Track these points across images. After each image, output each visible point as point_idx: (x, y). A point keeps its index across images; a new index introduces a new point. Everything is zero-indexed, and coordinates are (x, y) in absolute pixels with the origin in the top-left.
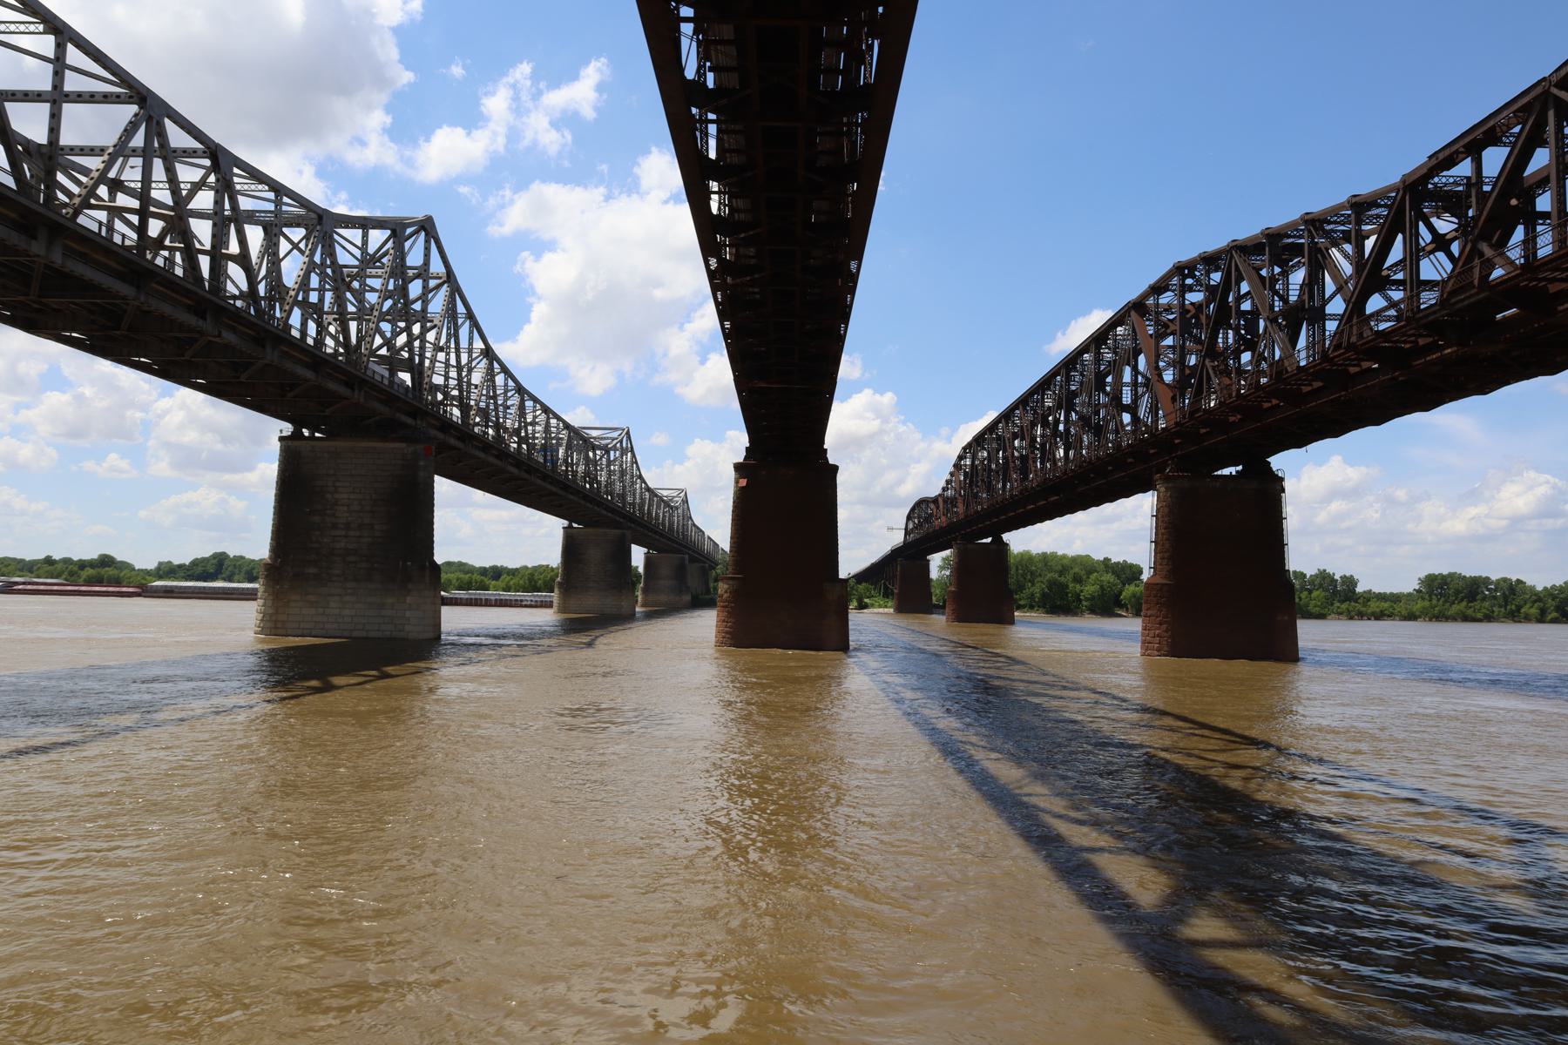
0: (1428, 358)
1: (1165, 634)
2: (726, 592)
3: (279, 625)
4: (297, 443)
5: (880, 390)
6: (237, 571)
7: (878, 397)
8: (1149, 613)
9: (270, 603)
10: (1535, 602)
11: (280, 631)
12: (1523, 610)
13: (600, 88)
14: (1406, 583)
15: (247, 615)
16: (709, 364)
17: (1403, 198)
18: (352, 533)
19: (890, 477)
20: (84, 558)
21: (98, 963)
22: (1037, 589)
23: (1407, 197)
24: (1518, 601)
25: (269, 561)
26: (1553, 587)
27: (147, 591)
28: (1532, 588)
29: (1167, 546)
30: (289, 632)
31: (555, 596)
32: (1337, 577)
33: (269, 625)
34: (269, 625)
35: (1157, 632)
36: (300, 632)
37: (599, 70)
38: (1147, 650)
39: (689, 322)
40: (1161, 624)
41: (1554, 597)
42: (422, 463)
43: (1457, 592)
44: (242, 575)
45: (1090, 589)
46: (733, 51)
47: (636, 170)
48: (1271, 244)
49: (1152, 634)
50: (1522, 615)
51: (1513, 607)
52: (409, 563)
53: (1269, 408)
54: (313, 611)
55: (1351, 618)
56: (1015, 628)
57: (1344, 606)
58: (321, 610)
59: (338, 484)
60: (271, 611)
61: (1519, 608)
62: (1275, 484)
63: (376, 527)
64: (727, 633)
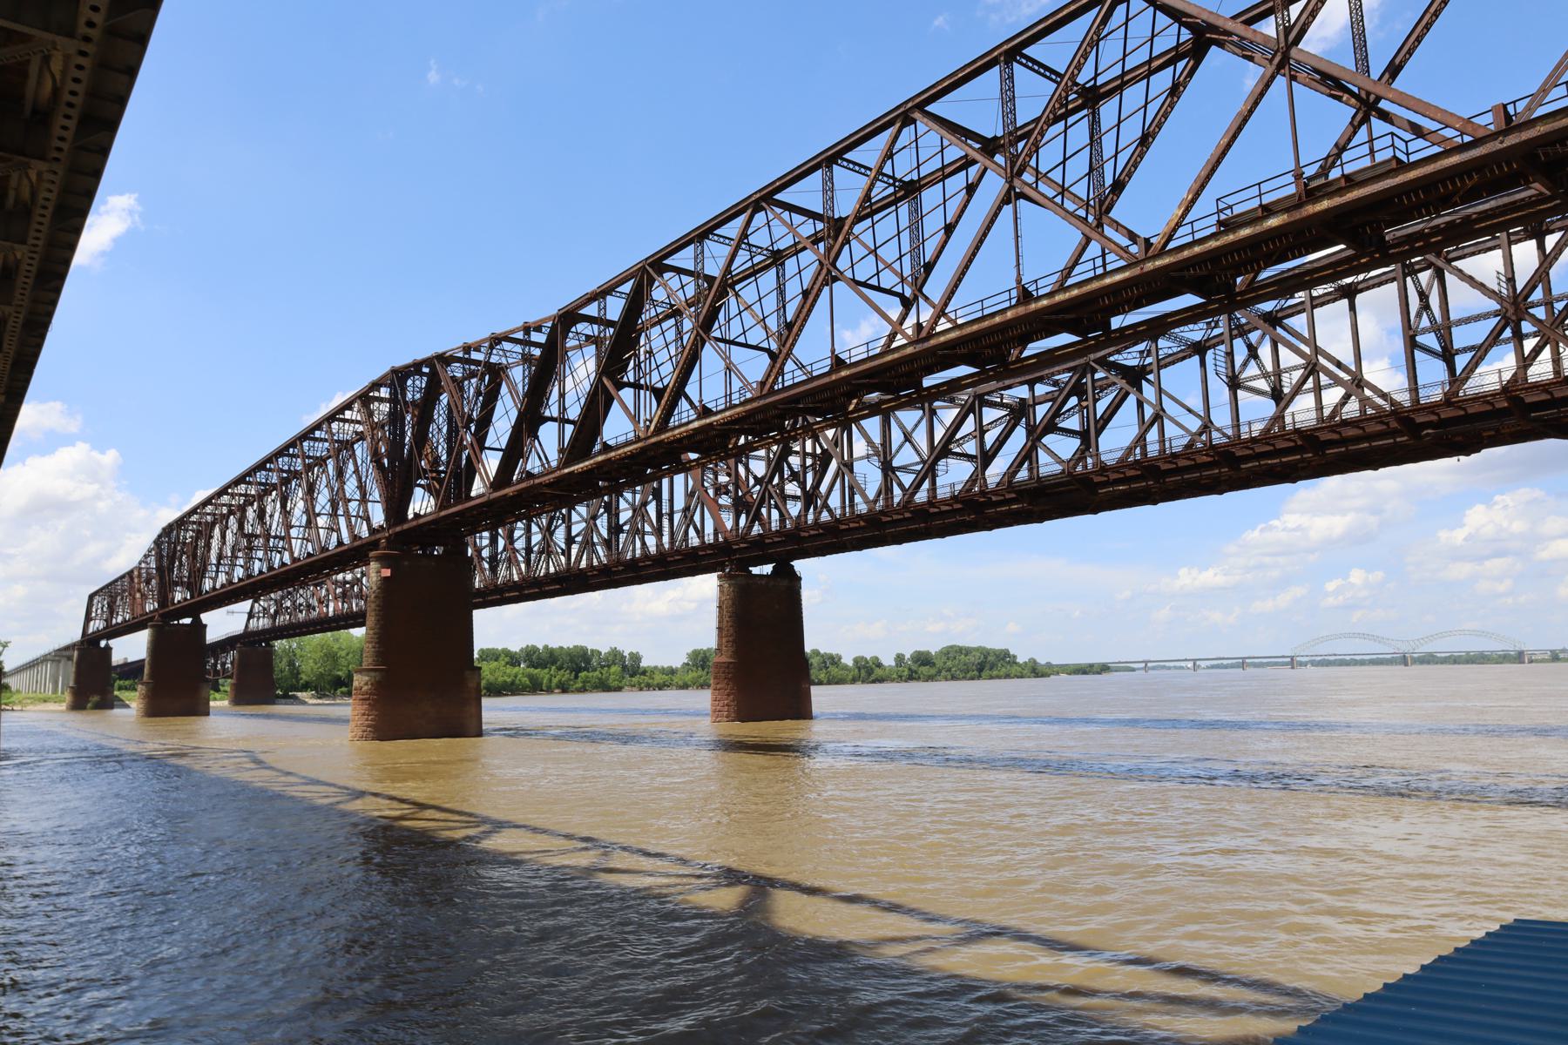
2: (366, 684)
5: (100, 446)
7: (96, 454)
8: (718, 686)
14: (678, 660)
17: (973, 402)
19: (93, 549)
21: (841, 969)
29: (731, 631)
32: (626, 654)
40: (728, 695)
49: (721, 703)
55: (641, 689)
57: (635, 680)
64: (368, 726)
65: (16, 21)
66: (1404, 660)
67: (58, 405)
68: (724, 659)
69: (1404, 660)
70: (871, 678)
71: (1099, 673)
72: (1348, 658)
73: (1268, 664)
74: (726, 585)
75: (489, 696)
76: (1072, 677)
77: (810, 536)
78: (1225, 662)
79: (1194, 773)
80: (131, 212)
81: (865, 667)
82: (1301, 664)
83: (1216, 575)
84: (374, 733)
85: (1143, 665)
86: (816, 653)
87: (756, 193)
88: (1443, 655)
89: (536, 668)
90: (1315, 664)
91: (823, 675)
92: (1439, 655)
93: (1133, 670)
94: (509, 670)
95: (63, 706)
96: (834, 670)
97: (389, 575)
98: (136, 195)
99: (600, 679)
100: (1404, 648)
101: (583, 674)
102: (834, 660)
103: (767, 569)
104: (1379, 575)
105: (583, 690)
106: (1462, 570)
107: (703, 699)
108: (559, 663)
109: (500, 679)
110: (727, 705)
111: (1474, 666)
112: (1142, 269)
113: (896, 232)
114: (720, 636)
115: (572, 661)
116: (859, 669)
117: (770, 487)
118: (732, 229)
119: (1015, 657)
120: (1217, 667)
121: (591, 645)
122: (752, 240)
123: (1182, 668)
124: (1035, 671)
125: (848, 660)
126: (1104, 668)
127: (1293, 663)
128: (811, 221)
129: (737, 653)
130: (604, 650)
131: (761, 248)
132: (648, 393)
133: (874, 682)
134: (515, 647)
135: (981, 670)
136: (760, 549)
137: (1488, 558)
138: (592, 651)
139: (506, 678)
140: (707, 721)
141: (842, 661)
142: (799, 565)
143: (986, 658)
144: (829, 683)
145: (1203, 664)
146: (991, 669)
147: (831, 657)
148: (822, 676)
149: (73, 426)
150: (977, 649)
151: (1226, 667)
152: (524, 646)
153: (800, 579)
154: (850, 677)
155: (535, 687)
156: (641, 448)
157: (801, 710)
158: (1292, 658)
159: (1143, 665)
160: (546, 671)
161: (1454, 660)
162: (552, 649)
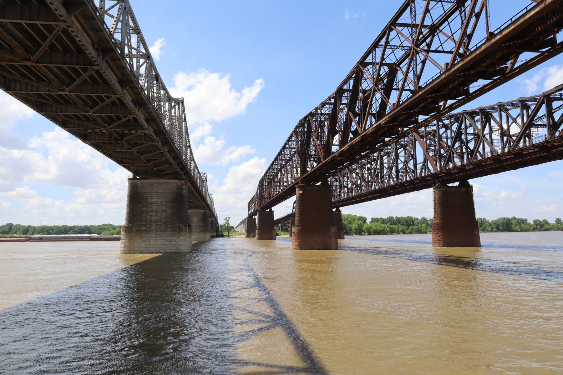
0: (558, 149)
1: (441, 239)
2: (296, 231)
3: (131, 249)
4: (135, 181)
6: (18, 230)
7: (260, 160)
8: (435, 232)
9: (127, 241)
10: (490, 225)
11: (131, 252)
12: (486, 228)
13: (161, 49)
15: (117, 246)
16: (199, 149)
18: (158, 214)
20: (82, 225)
23: (545, 99)
24: (484, 225)
25: (126, 225)
26: (494, 220)
27: (31, 239)
28: (488, 221)
29: (439, 210)
30: (135, 252)
31: (122, 236)
32: (428, 219)
33: (127, 249)
34: (127, 249)
35: (438, 239)
36: (147, 251)
37: (161, 43)
38: (435, 245)
39: (192, 133)
40: (439, 236)
41: (495, 224)
42: (184, 187)
44: (20, 232)
45: (355, 226)
47: (173, 79)
48: (481, 112)
49: (436, 239)
50: (486, 230)
51: (483, 227)
52: (181, 224)
54: (144, 243)
58: (147, 243)
59: (152, 196)
61: (485, 228)
62: (469, 189)
63: (168, 211)
65: (47, 21)
67: (248, 146)
68: (437, 221)
70: (544, 229)
74: (437, 191)
75: (375, 235)
77: (470, 169)
79: (243, 299)
80: (261, 84)
81: (539, 224)
84: (299, 247)
87: (389, 23)
89: (392, 224)
91: (518, 228)
94: (382, 225)
95: (244, 236)
96: (523, 226)
97: (301, 193)
98: (262, 79)
99: (418, 229)
101: (411, 227)
102: (523, 222)
103: (456, 184)
105: (411, 233)
107: (429, 237)
108: (401, 223)
109: (379, 229)
110: (439, 240)
112: (545, 4)
113: (450, 24)
114: (435, 212)
115: (407, 222)
116: (536, 225)
117: (453, 149)
118: (383, 42)
121: (414, 216)
122: (391, 43)
125: (531, 221)
128: (406, 28)
130: (420, 217)
131: (397, 46)
132: (371, 116)
133: (544, 230)
134: (385, 217)
136: (450, 175)
138: (415, 218)
139: (381, 228)
140: (430, 246)
141: (528, 221)
142: (471, 182)
144: (521, 231)
147: (522, 220)
148: (517, 228)
149: (253, 152)
152: (388, 217)
153: (472, 187)
154: (532, 228)
155: (392, 232)
157: (475, 243)
160: (397, 226)
162: (399, 218)
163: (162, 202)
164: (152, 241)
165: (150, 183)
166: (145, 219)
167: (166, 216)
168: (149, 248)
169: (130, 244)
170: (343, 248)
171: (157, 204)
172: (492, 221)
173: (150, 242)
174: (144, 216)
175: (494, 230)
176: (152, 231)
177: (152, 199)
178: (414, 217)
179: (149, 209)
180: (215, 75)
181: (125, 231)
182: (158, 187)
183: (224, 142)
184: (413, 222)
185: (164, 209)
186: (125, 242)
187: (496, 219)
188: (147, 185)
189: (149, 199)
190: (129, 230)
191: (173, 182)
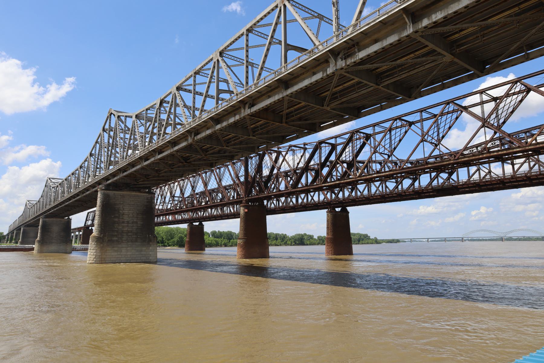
2: (242, 242)
3: (103, 260)
10: (290, 240)
11: (103, 262)
18: (130, 225)
22: (176, 239)
24: (286, 240)
30: (107, 262)
33: (98, 259)
40: (331, 247)
43: (273, 238)
46: (515, 163)
53: (372, 199)
54: (116, 253)
56: (206, 251)
58: (119, 253)
59: (124, 207)
60: (99, 254)
61: (286, 242)
63: (138, 223)
66: (502, 239)
67: (44, 147)
68: (330, 237)
69: (502, 239)
71: (396, 243)
72: (481, 238)
73: (452, 240)
76: (387, 244)
78: (456, 239)
81: (321, 239)
82: (466, 240)
83: (433, 208)
85: (427, 240)
86: (206, 232)
88: (515, 238)
89: (217, 238)
90: (469, 240)
92: (513, 238)
93: (405, 242)
100: (502, 235)
101: (232, 240)
102: (311, 237)
104: (491, 209)
105: (232, 246)
106: (520, 208)
107: (323, 248)
111: (526, 241)
116: (320, 240)
119: (369, 237)
120: (434, 241)
123: (422, 241)
124: (376, 241)
125: (316, 237)
126: (398, 241)
127: (462, 240)
129: (333, 235)
135: (359, 241)
137: (530, 203)
142: (349, 208)
143: (361, 237)
144: (310, 245)
145: (429, 240)
146: (362, 240)
148: (308, 242)
150: (358, 234)
151: (437, 241)
152: (212, 231)
153: (349, 212)
154: (317, 243)
156: (353, 181)
158: (462, 238)
159: (410, 240)
161: (519, 239)
163: (134, 214)
164: (123, 251)
165: (122, 195)
166: (116, 229)
167: (136, 227)
168: (120, 258)
169: (102, 255)
170: (156, 262)
171: (128, 215)
172: (291, 236)
173: (121, 252)
174: (116, 227)
175: (293, 244)
176: (124, 241)
177: (124, 210)
178: (303, 234)
179: (121, 220)
180: (14, 62)
181: (96, 241)
182: (130, 199)
183: (11, 138)
184: (232, 236)
185: (135, 221)
186: (96, 252)
187: (294, 235)
188: (119, 197)
189: (121, 210)
190: (101, 240)
191: (143, 195)
